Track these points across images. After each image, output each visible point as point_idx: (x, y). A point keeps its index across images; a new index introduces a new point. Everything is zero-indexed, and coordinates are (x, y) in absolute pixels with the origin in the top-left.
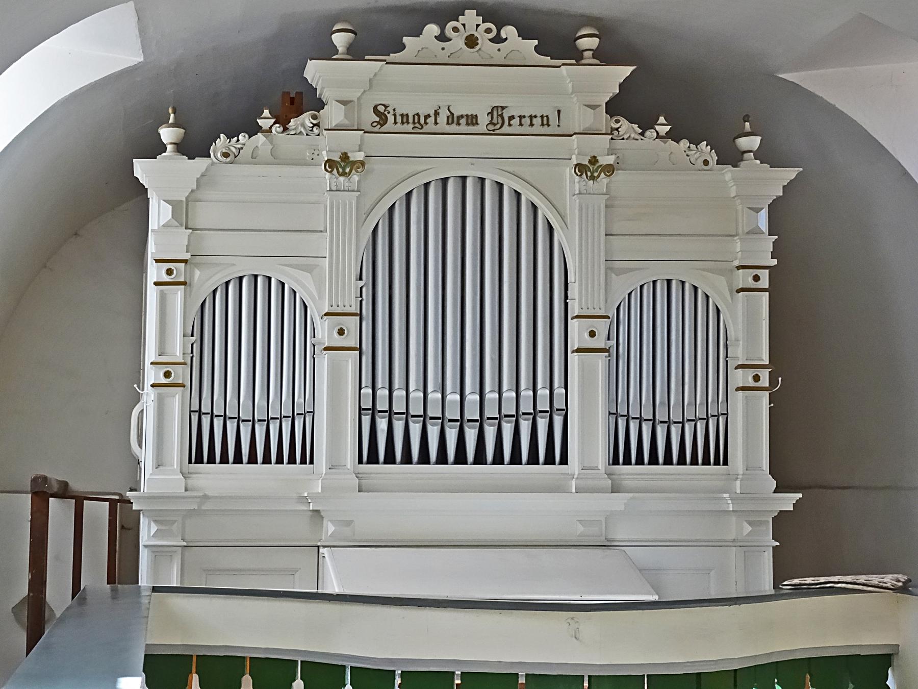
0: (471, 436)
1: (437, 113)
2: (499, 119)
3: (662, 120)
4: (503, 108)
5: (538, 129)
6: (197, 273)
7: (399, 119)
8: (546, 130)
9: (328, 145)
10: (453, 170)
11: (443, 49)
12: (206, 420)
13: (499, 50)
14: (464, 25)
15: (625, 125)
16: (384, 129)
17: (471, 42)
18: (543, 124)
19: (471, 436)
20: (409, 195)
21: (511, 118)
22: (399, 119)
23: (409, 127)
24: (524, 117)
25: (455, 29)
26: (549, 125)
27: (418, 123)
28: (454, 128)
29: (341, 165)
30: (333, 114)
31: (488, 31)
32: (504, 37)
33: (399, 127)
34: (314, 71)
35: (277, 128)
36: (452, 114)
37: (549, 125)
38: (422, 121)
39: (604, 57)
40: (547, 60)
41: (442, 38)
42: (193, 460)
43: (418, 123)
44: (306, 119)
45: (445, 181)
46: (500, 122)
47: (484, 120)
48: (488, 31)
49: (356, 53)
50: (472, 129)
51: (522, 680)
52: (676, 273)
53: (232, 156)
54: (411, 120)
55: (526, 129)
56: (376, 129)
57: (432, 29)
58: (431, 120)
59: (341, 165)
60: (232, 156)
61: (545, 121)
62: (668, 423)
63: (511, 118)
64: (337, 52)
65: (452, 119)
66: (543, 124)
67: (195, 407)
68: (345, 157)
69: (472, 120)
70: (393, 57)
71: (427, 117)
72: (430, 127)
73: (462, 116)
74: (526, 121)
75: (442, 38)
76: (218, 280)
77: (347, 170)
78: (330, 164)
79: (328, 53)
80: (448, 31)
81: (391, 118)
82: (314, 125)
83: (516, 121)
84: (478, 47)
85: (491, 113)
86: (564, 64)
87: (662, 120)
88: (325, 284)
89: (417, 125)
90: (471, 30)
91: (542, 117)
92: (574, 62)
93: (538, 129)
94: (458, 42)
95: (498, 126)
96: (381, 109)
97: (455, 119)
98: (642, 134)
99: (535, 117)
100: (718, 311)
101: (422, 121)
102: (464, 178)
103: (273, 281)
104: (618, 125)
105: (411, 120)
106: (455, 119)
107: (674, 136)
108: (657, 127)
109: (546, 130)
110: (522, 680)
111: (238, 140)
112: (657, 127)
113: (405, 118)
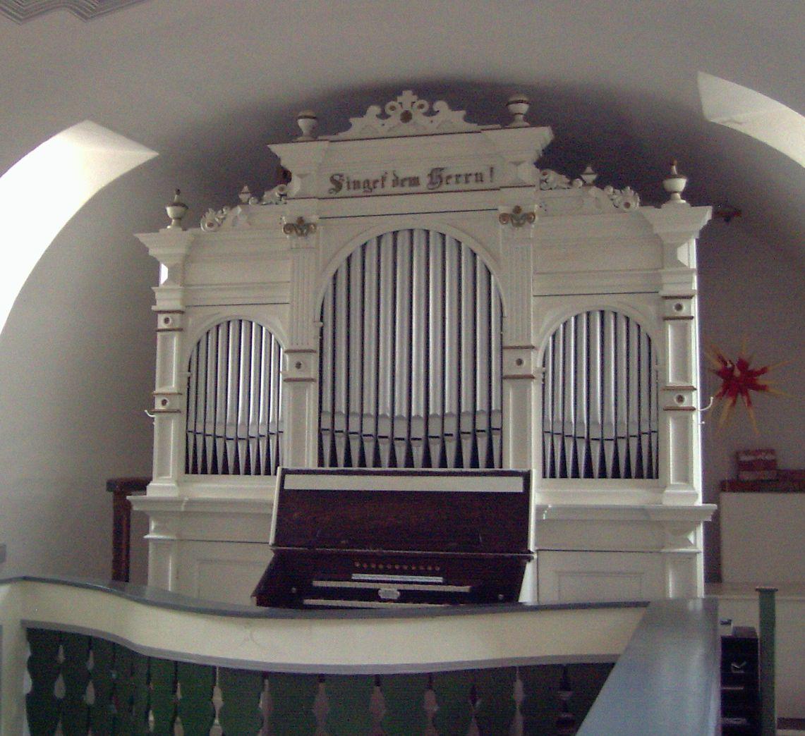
0: (418, 453)
1: (384, 179)
2: (438, 178)
3: (589, 169)
4: (442, 169)
5: (473, 185)
6: (190, 321)
7: (352, 186)
8: (480, 186)
9: (289, 212)
10: (409, 222)
11: (383, 125)
12: (200, 439)
13: (432, 122)
14: (401, 103)
15: (552, 176)
16: (339, 194)
17: (406, 117)
18: (477, 180)
19: (418, 453)
20: (364, 247)
21: (449, 177)
22: (352, 186)
23: (360, 192)
24: (460, 176)
25: (393, 108)
26: (482, 181)
27: (369, 188)
28: (398, 189)
29: (300, 227)
30: (295, 186)
31: (421, 107)
32: (436, 110)
33: (353, 192)
34: (287, 154)
35: (252, 201)
36: (397, 178)
37: (482, 181)
38: (371, 186)
39: (534, 120)
40: (474, 127)
41: (383, 115)
42: (190, 471)
43: (369, 188)
44: (276, 192)
45: (395, 234)
46: (439, 181)
47: (424, 181)
48: (421, 107)
49: (315, 136)
50: (414, 189)
51: (703, 423)
52: (608, 303)
53: (216, 226)
54: (362, 185)
55: (462, 186)
56: (332, 195)
57: (374, 110)
58: (379, 185)
59: (300, 227)
60: (216, 226)
61: (479, 177)
62: (602, 441)
63: (449, 177)
64: (301, 134)
65: (397, 182)
66: (477, 180)
67: (191, 428)
68: (301, 220)
69: (415, 181)
70: (342, 135)
71: (376, 181)
72: (378, 190)
73: (405, 179)
74: (462, 179)
75: (383, 115)
76: (209, 324)
77: (305, 231)
78: (289, 228)
79: (291, 135)
80: (389, 112)
81: (345, 185)
82: (281, 196)
83: (462, 179)
84: (412, 121)
85: (431, 175)
86: (483, 130)
87: (589, 169)
88: (285, 324)
89: (367, 189)
90: (407, 107)
91: (476, 174)
92: (498, 126)
93: (473, 185)
94: (395, 119)
95: (437, 185)
96: (337, 178)
97: (400, 181)
98: (570, 183)
99: (470, 175)
100: (649, 340)
101: (371, 186)
102: (411, 231)
103: (254, 324)
104: (546, 177)
105: (362, 185)
106: (400, 181)
107: (600, 183)
108: (584, 177)
109: (480, 186)
110: (703, 423)
111: (223, 212)
112: (584, 177)
113: (357, 184)
